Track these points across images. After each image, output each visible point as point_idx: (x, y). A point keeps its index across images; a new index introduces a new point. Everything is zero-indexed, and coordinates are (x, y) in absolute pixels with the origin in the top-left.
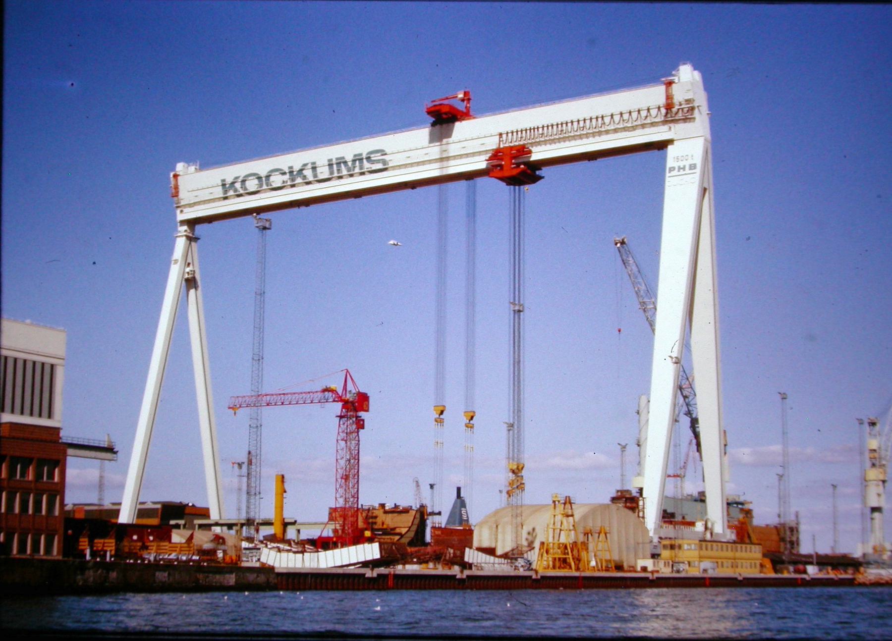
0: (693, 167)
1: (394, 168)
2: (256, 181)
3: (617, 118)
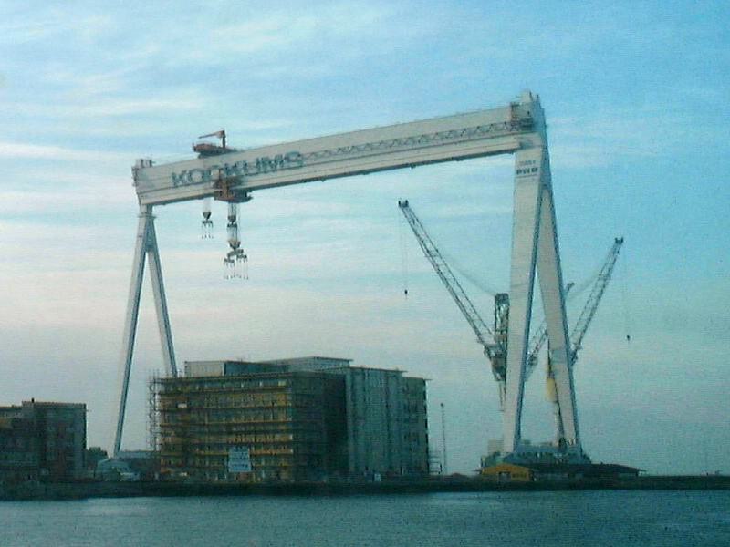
0: (535, 170)
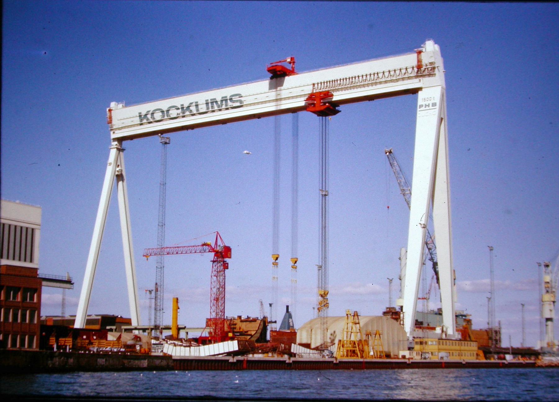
0: (434, 105)
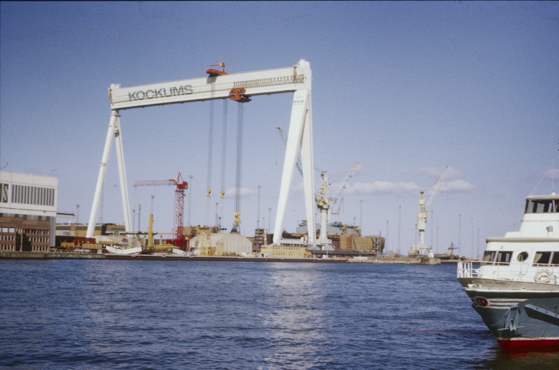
0: (302, 101)
1: (195, 93)
2: (142, 95)
3: (276, 80)
